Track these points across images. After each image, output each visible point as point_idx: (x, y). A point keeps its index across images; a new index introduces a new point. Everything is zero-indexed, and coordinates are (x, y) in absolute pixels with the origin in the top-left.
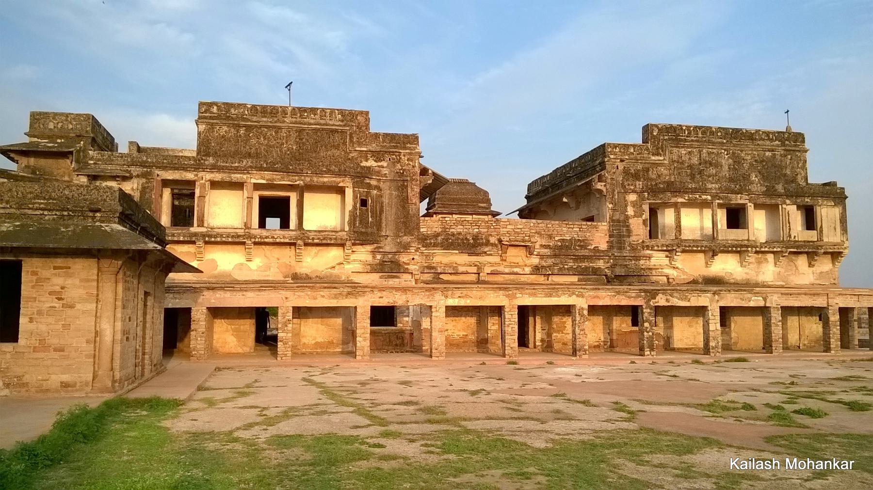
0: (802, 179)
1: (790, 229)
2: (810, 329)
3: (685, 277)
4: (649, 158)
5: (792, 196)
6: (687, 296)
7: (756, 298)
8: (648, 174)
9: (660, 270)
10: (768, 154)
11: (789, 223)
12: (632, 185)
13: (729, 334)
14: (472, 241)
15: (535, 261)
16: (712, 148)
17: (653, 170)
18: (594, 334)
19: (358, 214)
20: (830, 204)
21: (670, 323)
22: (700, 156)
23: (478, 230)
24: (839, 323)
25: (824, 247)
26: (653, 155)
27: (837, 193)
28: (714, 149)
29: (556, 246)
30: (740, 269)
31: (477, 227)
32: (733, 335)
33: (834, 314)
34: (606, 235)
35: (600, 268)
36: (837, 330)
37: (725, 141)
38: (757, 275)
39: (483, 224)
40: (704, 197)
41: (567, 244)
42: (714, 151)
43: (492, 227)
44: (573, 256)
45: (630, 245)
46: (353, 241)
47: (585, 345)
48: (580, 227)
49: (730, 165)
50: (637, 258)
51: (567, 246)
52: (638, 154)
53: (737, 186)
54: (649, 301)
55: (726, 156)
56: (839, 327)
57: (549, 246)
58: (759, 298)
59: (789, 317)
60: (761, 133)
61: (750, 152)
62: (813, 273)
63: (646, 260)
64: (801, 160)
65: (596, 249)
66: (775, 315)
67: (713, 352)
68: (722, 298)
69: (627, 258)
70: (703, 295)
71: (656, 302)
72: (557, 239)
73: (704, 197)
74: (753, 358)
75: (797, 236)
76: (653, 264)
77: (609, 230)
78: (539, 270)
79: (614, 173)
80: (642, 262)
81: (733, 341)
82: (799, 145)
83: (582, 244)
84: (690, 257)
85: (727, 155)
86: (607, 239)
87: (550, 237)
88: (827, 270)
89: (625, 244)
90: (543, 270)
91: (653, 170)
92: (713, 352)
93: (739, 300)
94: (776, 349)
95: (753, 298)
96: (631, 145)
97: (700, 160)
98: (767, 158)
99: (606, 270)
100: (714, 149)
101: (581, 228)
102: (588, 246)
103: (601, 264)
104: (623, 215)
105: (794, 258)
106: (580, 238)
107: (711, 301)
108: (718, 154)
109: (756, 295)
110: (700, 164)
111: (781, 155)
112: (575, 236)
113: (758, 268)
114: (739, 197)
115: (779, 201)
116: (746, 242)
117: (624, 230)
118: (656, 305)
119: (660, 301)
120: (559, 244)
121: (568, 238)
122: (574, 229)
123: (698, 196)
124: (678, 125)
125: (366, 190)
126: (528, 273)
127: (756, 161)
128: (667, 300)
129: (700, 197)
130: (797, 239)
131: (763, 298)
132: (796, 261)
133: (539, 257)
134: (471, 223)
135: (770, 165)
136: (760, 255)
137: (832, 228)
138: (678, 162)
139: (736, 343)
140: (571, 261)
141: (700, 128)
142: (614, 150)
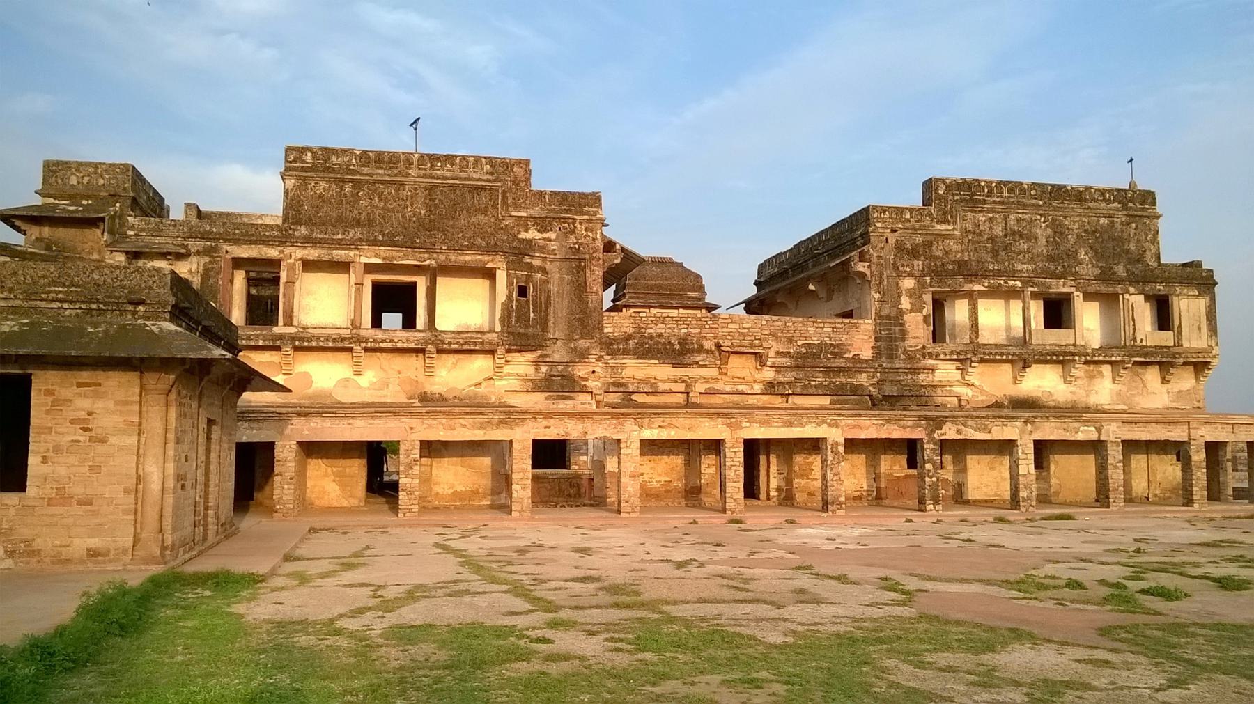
1: (1134, 329)
2: (1164, 473)
3: (984, 398)
4: (933, 227)
5: (1138, 282)
6: (987, 425)
7: (1086, 428)
8: (930, 250)
9: (948, 388)
10: (1103, 221)
11: (1134, 320)
12: (908, 265)
13: (1047, 480)
14: (678, 347)
15: (769, 374)
16: (1023, 213)
17: (938, 244)
18: (853, 480)
19: (514, 307)
20: (1192, 293)
21: (962, 465)
22: (1006, 224)
23: (686, 331)
24: (1205, 464)
26: (938, 222)
27: (1203, 277)
28: (1026, 213)
29: (798, 353)
30: (1062, 387)
31: (686, 326)
32: (1053, 481)
33: (1198, 451)
34: (870, 337)
35: (862, 385)
36: (1203, 474)
37: (1041, 203)
38: (1088, 395)
39: (694, 322)
40: (1011, 283)
41: (814, 351)
42: (1026, 217)
43: (707, 326)
44: (823, 367)
45: (905, 351)
46: (507, 347)
47: (840, 496)
48: (833, 326)
49: (1049, 237)
50: (915, 371)
53: (1059, 268)
54: (932, 432)
55: (1043, 225)
56: (1205, 471)
57: (789, 353)
58: (1090, 428)
59: (1133, 456)
60: (1093, 190)
61: (1078, 219)
62: (1168, 393)
63: (928, 373)
64: (1150, 230)
65: (856, 358)
66: (1113, 453)
67: (1025, 506)
68: (1037, 429)
69: (901, 370)
70: (1009, 424)
71: (942, 435)
72: (800, 343)
73: (1011, 283)
74: (1082, 514)
75: (1144, 339)
76: (938, 379)
77: (875, 331)
78: (774, 387)
79: (882, 248)
80: (922, 376)
81: (1053, 490)
84: (991, 369)
85: (1044, 222)
86: (872, 344)
87: (791, 340)
88: (1188, 388)
89: (897, 350)
90: (781, 388)
91: (938, 244)
93: (1062, 431)
94: (1114, 502)
95: (1082, 429)
97: (1006, 229)
98: (1102, 226)
99: (871, 388)
100: (1026, 213)
101: (835, 327)
102: (845, 353)
103: (863, 379)
104: (895, 309)
105: (1140, 371)
106: (834, 343)
107: (1022, 432)
109: (1087, 424)
110: (1006, 236)
113: (1089, 385)
114: (1062, 283)
115: (1119, 289)
117: (897, 331)
118: (943, 437)
120: (804, 350)
121: (816, 342)
122: (825, 329)
123: (1002, 282)
124: (974, 180)
125: (526, 273)
126: (759, 392)
127: (1086, 231)
128: (959, 432)
129: (1006, 283)
130: (1144, 343)
131: (1096, 428)
132: (1144, 375)
133: (774, 369)
134: (677, 321)
135: (1106, 236)
136: (1092, 367)
137: (1196, 327)
138: (974, 233)
139: (1057, 493)
140: (821, 375)
141: (1006, 183)
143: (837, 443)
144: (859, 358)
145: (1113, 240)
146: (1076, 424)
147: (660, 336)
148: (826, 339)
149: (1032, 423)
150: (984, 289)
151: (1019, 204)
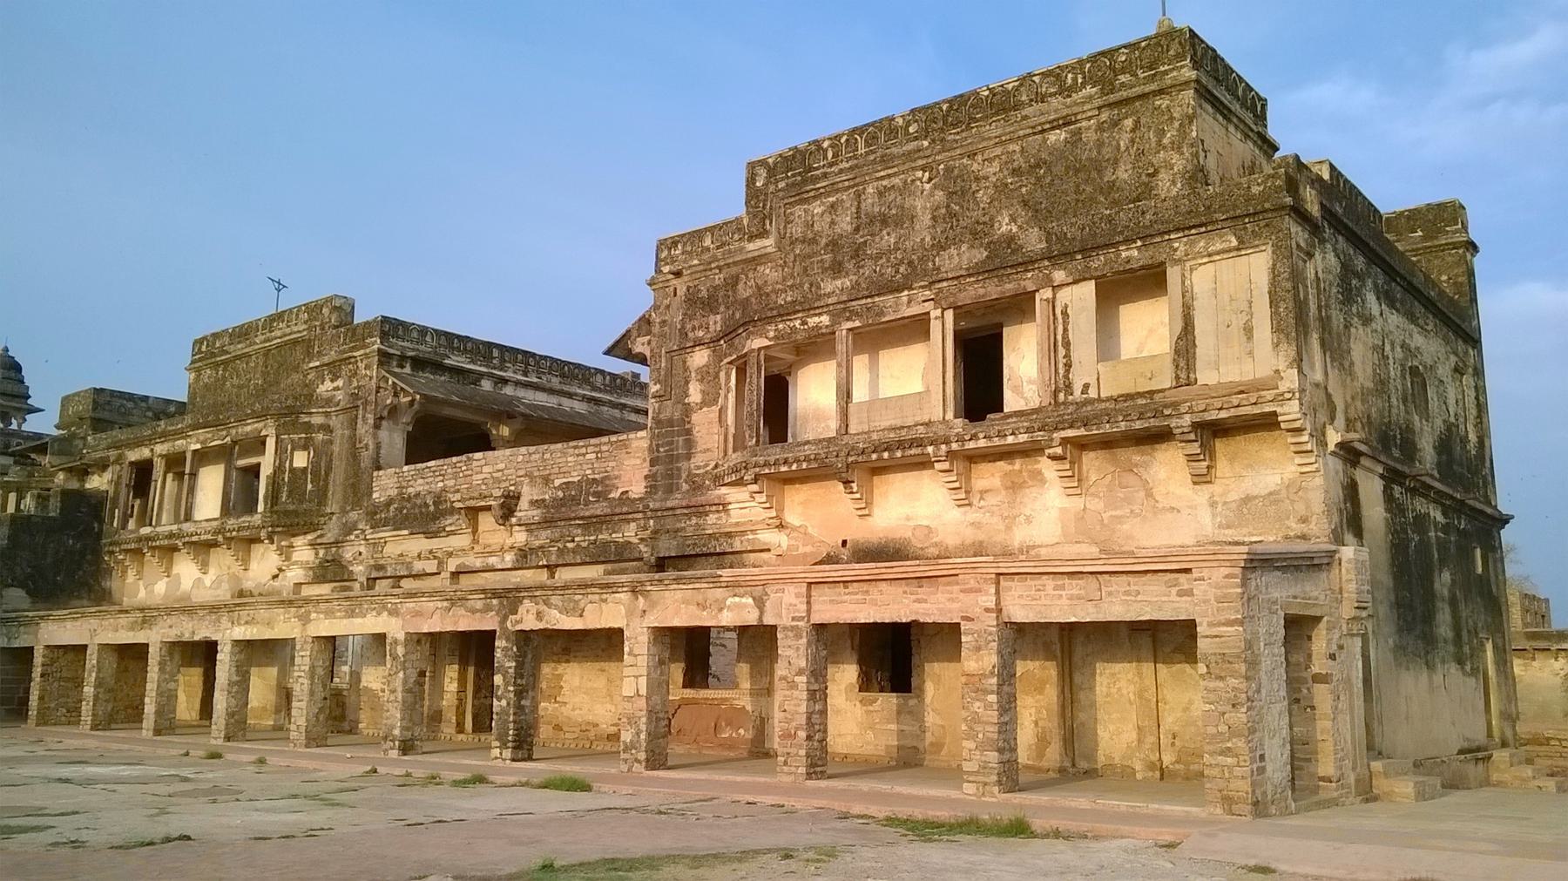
0: (1174, 183)
1: (1068, 366)
2: (1186, 709)
3: (808, 549)
4: (742, 249)
5: (1068, 255)
6: (576, 602)
7: (737, 599)
8: (734, 292)
9: (751, 537)
10: (1057, 137)
11: (1067, 345)
12: (700, 327)
13: (917, 715)
14: (432, 508)
15: (520, 537)
16: (889, 176)
17: (747, 276)
18: (609, 706)
19: (286, 479)
20: (1219, 246)
21: (766, 680)
22: (859, 208)
24: (994, 680)
25: (1184, 408)
26: (751, 238)
28: (894, 174)
29: (555, 499)
30: (955, 514)
31: (441, 478)
32: (931, 719)
33: (978, 649)
34: (645, 460)
35: (630, 542)
36: (988, 706)
37: (926, 143)
38: (1009, 528)
39: (449, 471)
40: (813, 321)
41: (573, 493)
42: (896, 181)
43: (461, 475)
44: (578, 519)
45: (691, 478)
46: (270, 529)
47: (393, 727)
48: (598, 449)
49: (938, 208)
50: (700, 510)
52: (718, 248)
53: (902, 269)
54: (505, 618)
55: (927, 186)
56: (993, 698)
57: (543, 500)
58: (744, 600)
59: (1099, 666)
60: (1036, 79)
62: (1213, 504)
63: (718, 511)
64: (1172, 119)
65: (624, 498)
66: (789, 652)
67: (626, 761)
68: (653, 605)
69: (678, 512)
70: (610, 597)
71: (517, 622)
72: (557, 483)
73: (813, 321)
74: (604, 778)
75: (1093, 382)
76: (733, 521)
77: (650, 449)
78: (526, 557)
79: (668, 307)
80: (711, 519)
81: (929, 738)
82: (1166, 73)
83: (600, 488)
84: (821, 491)
85: (930, 179)
86: (646, 472)
87: (547, 480)
88: (1272, 488)
89: (679, 477)
90: (534, 556)
91: (747, 276)
92: (626, 761)
93: (693, 608)
94: (785, 763)
95: (730, 601)
96: (706, 229)
97: (858, 218)
98: (1053, 150)
99: (641, 547)
100: (894, 174)
101: (600, 452)
102: (610, 492)
104: (680, 406)
105: (1137, 458)
106: (597, 476)
107: (630, 614)
108: (905, 189)
109: (737, 590)
110: (857, 229)
111: (1100, 128)
112: (588, 472)
113: (1012, 504)
114: (905, 299)
115: (1028, 282)
117: (681, 443)
118: (518, 627)
120: (560, 494)
121: (576, 479)
122: (588, 457)
123: (797, 323)
124: (810, 144)
125: (303, 435)
126: (509, 566)
127: (1016, 172)
128: (539, 616)
129: (804, 323)
130: (1093, 394)
131: (754, 599)
132: (1146, 465)
133: (523, 528)
134: (434, 472)
135: (1059, 169)
136: (1018, 464)
137: (1236, 331)
138: (803, 242)
139: (938, 746)
140: (579, 531)
141: (860, 130)
142: (673, 252)
143: (396, 642)
144: (628, 498)
145: (1077, 171)
146: (719, 593)
147: (418, 495)
149: (645, 593)
150: (768, 343)
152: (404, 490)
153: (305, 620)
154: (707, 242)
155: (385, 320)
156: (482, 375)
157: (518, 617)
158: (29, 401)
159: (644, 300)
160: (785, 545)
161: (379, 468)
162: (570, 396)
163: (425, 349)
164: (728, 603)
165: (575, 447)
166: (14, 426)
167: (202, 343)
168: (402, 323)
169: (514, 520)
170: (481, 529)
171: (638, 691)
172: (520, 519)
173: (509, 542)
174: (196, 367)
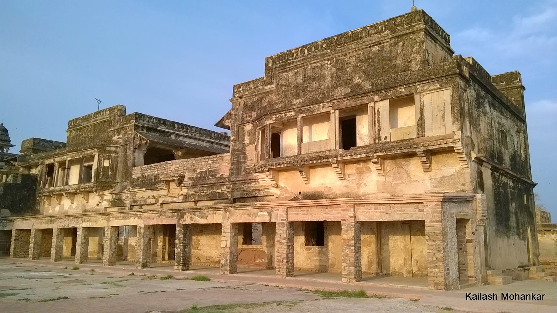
1: (379, 130)
2: (421, 252)
3: (287, 195)
4: (263, 88)
5: (379, 91)
6: (205, 214)
7: (262, 213)
8: (261, 104)
9: (267, 191)
10: (376, 49)
11: (379, 122)
12: (249, 116)
13: (326, 254)
14: (153, 181)
15: (185, 191)
16: (316, 62)
17: (265, 98)
18: (216, 251)
19: (102, 170)
20: (433, 87)
21: (272, 242)
22: (305, 74)
24: (353, 242)
26: (267, 85)
27: (445, 70)
28: (318, 62)
29: (197, 177)
30: (339, 183)
31: (157, 170)
32: (331, 255)
33: (348, 230)
34: (229, 163)
35: (224, 193)
36: (351, 251)
37: (329, 51)
38: (358, 188)
39: (160, 167)
40: (289, 114)
41: (204, 175)
42: (318, 64)
43: (164, 169)
44: (205, 184)
45: (245, 170)
46: (96, 188)
48: (212, 160)
49: (333, 74)
50: (249, 181)
51: (204, 177)
53: (320, 96)
54: (179, 220)
55: (329, 66)
56: (353, 248)
57: (193, 178)
58: (264, 213)
59: (390, 237)
60: (368, 28)
61: (355, 54)
62: (431, 179)
63: (255, 182)
64: (416, 42)
65: (222, 177)
66: (280, 232)
67: (222, 270)
68: (232, 215)
69: (241, 182)
70: (217, 212)
71: (184, 221)
72: (198, 171)
73: (289, 114)
74: (214, 277)
75: (388, 136)
76: (261, 185)
77: (231, 159)
78: (187, 198)
79: (237, 109)
80: (253, 184)
81: (330, 262)
84: (292, 175)
85: (330, 64)
86: (229, 168)
87: (194, 171)
88: (452, 173)
89: (241, 169)
90: (190, 198)
91: (265, 98)
93: (246, 216)
94: (279, 271)
95: (259, 213)
97: (305, 77)
98: (374, 53)
99: (228, 194)
100: (318, 62)
101: (213, 160)
102: (217, 175)
103: (224, 189)
104: (242, 144)
105: (404, 163)
106: (212, 169)
107: (224, 218)
109: (262, 210)
110: (304, 82)
113: (359, 179)
114: (321, 106)
115: (365, 100)
116: (327, 152)
117: (242, 157)
118: (184, 223)
119: (186, 220)
120: (199, 175)
121: (205, 170)
122: (209, 162)
123: (283, 115)
124: (288, 51)
125: (108, 155)
126: (181, 201)
127: (361, 61)
128: (192, 219)
129: (286, 115)
130: (388, 140)
131: (268, 213)
132: (407, 165)
133: (186, 188)
134: (154, 168)
135: (376, 60)
136: (362, 165)
137: (439, 117)
138: (285, 86)
139: (333, 265)
140: (206, 189)
141: (305, 46)
142: (239, 90)
147: (148, 176)
148: (209, 168)
149: (229, 211)
151: (315, 57)
152: (144, 174)
153: (108, 220)
154: (251, 86)
155: (137, 114)
156: (171, 133)
157: (184, 219)
158: (10, 143)
159: (229, 107)
160: (279, 194)
161: (135, 166)
162: (203, 141)
163: (151, 124)
164: (259, 214)
165: (204, 159)
166: (5, 151)
167: (72, 122)
168: (143, 115)
169: (182, 185)
170: (171, 188)
171: (227, 245)
172: (185, 185)
173: (181, 192)
174: (69, 130)
